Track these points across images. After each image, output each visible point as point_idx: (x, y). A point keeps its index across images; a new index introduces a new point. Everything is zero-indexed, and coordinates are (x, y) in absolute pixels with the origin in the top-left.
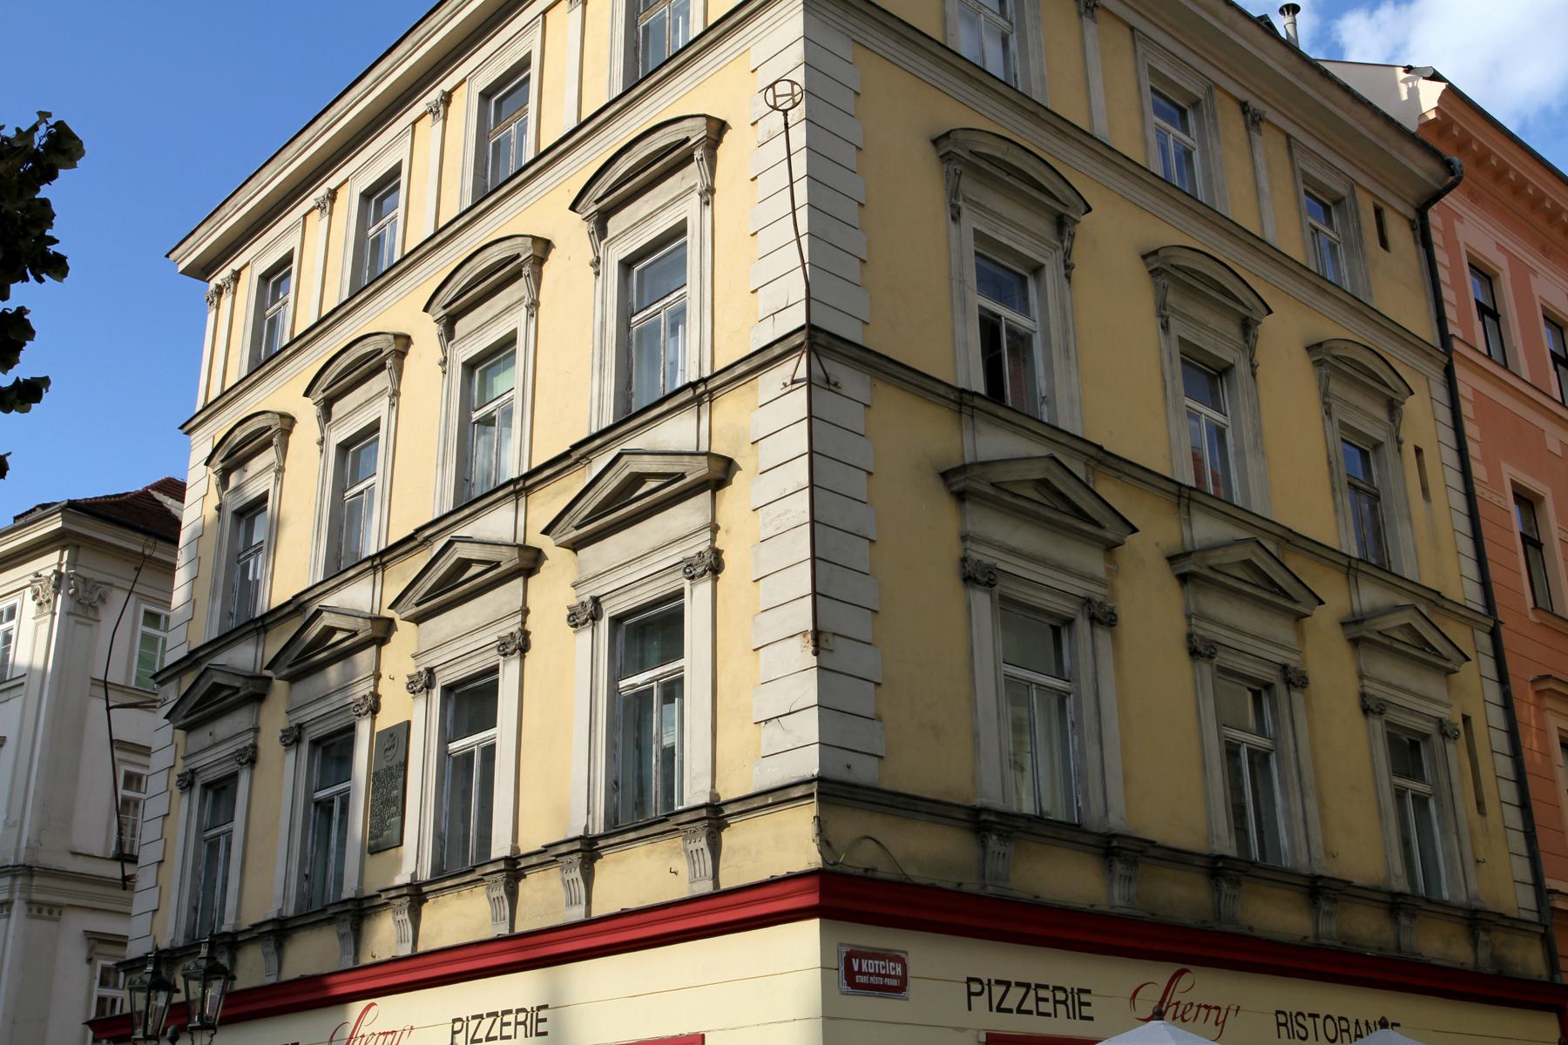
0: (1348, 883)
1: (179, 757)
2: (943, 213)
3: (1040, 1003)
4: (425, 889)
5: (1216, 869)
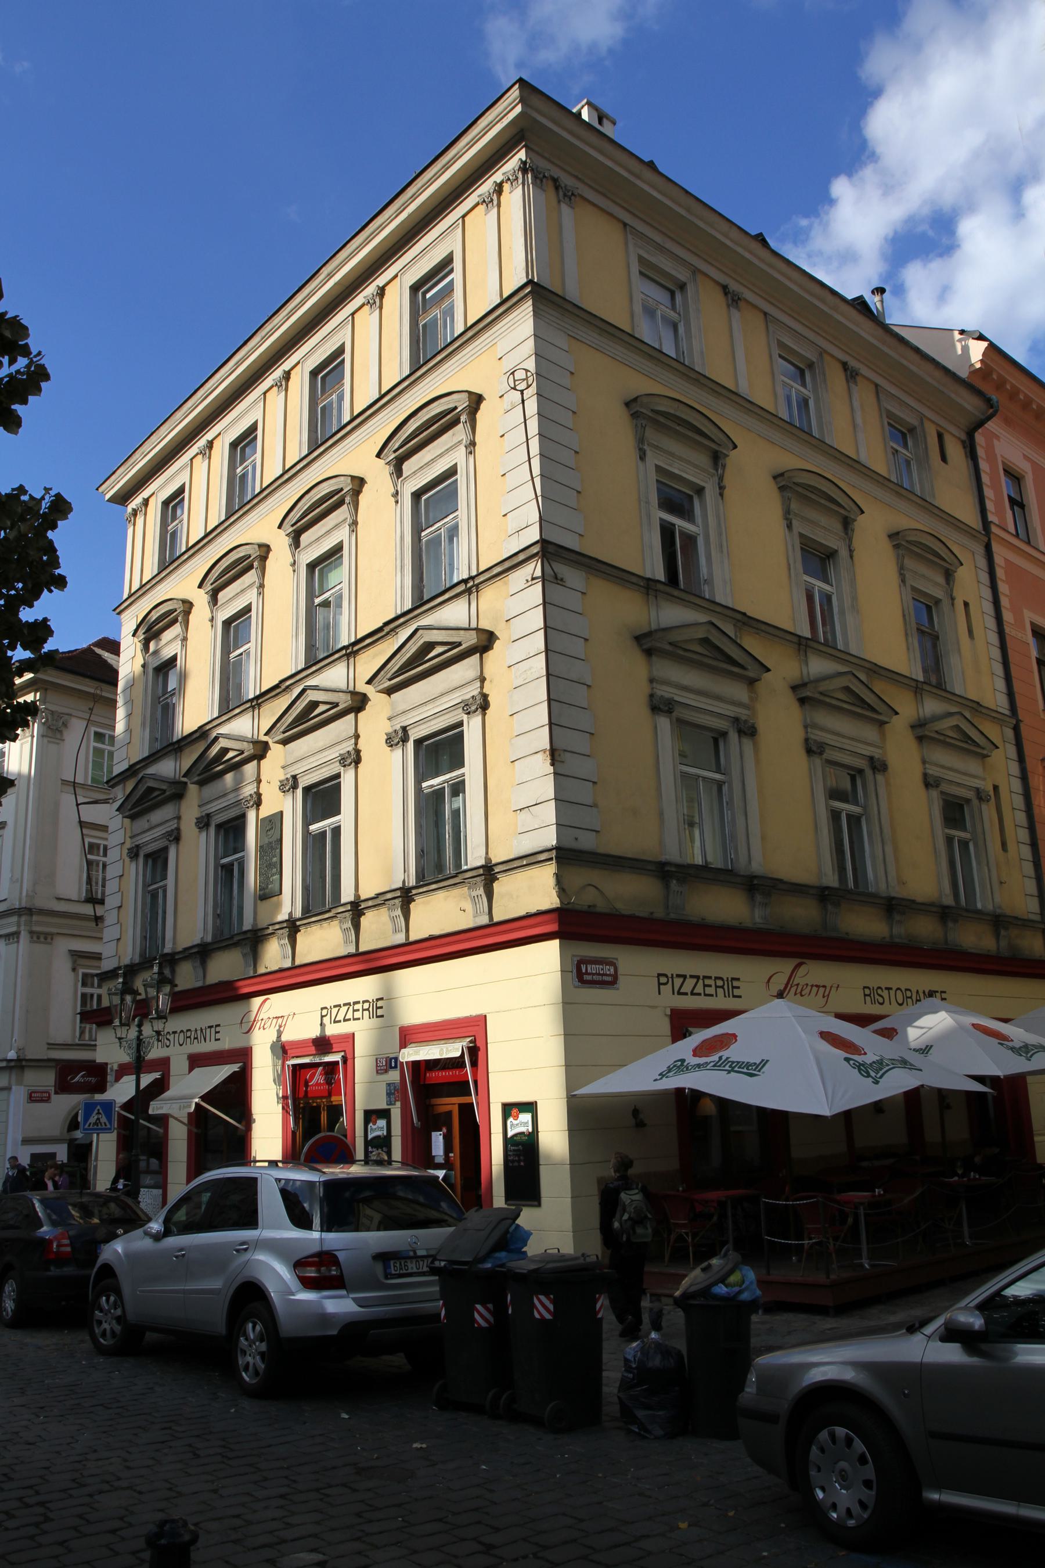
0: (913, 901)
1: (127, 836)
2: (634, 455)
3: (706, 988)
4: (298, 923)
5: (824, 895)
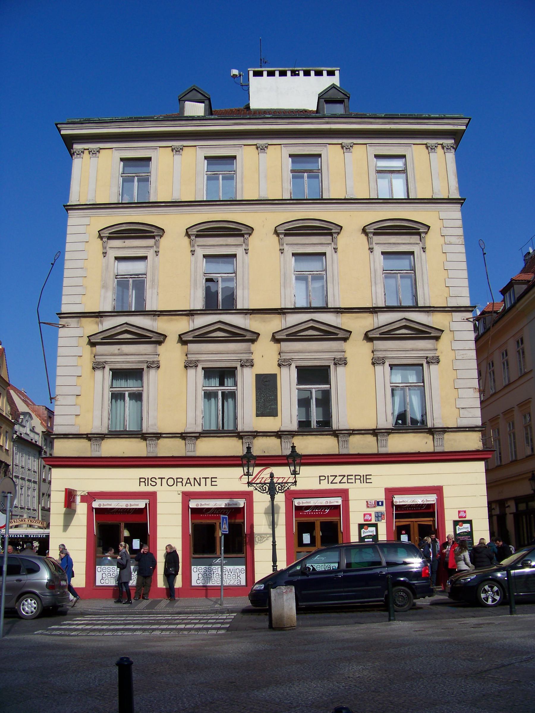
3: (349, 480)
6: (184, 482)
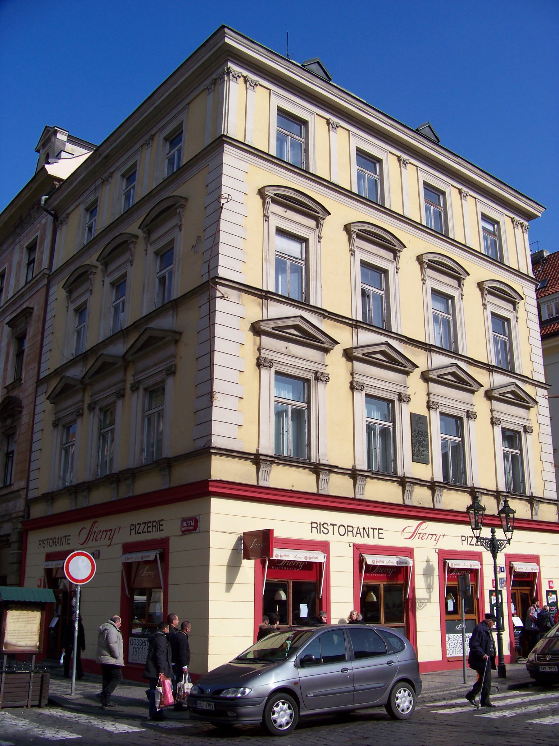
3: (380, 535)
6: (355, 532)
